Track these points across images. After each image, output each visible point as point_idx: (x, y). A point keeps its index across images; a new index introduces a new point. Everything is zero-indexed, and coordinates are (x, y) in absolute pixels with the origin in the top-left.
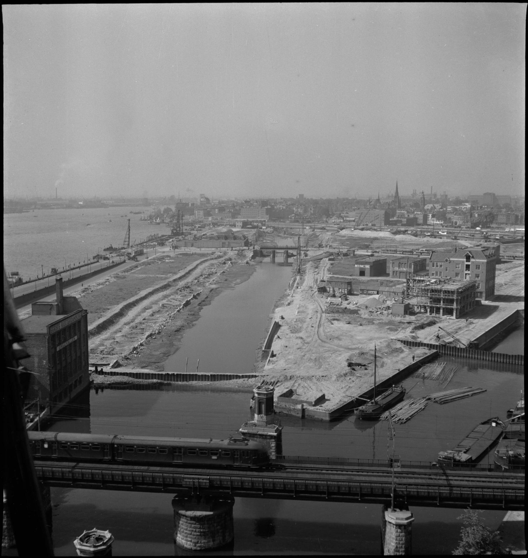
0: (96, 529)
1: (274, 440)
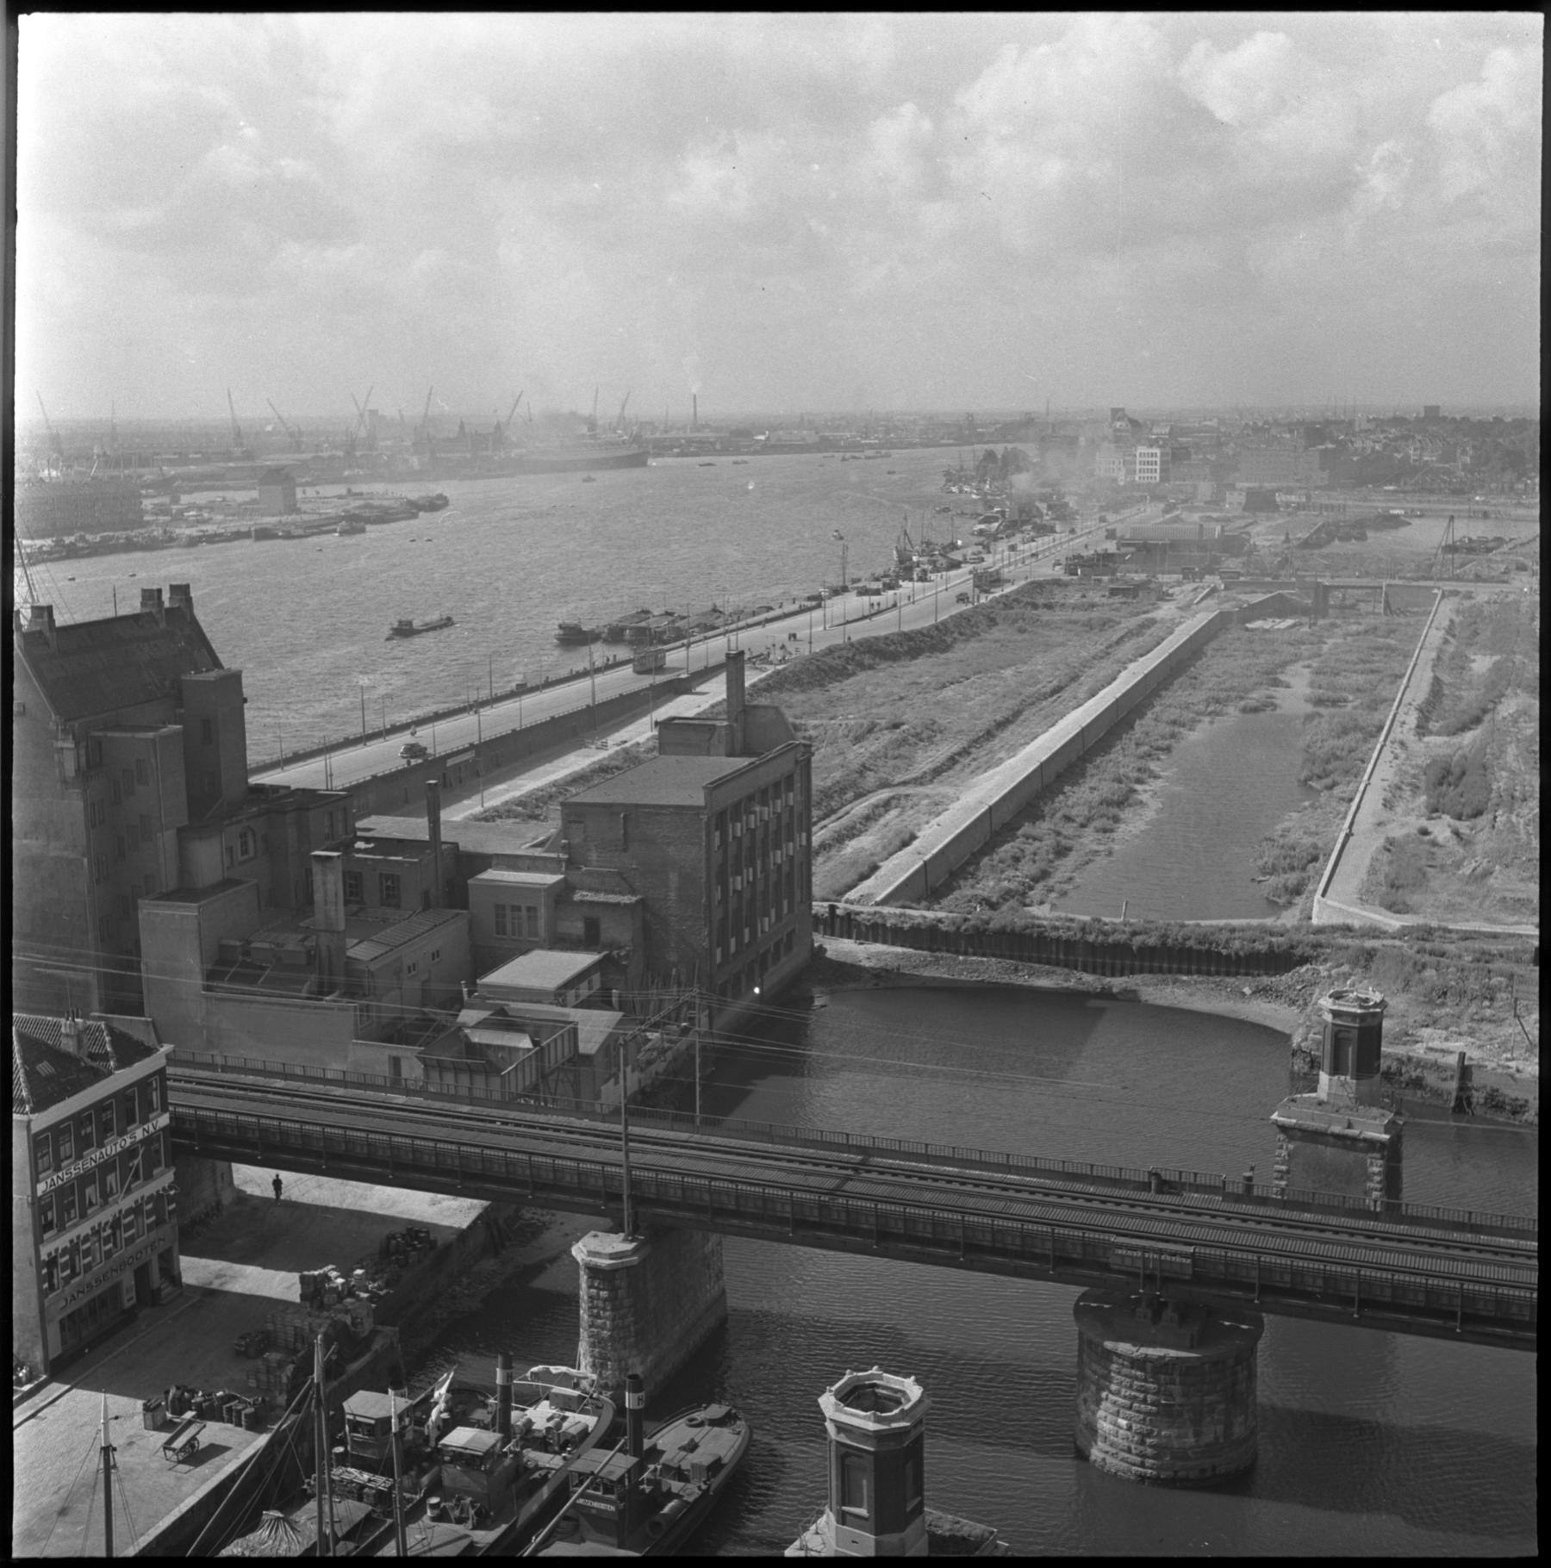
0: (880, 1369)
1: (1378, 1155)
